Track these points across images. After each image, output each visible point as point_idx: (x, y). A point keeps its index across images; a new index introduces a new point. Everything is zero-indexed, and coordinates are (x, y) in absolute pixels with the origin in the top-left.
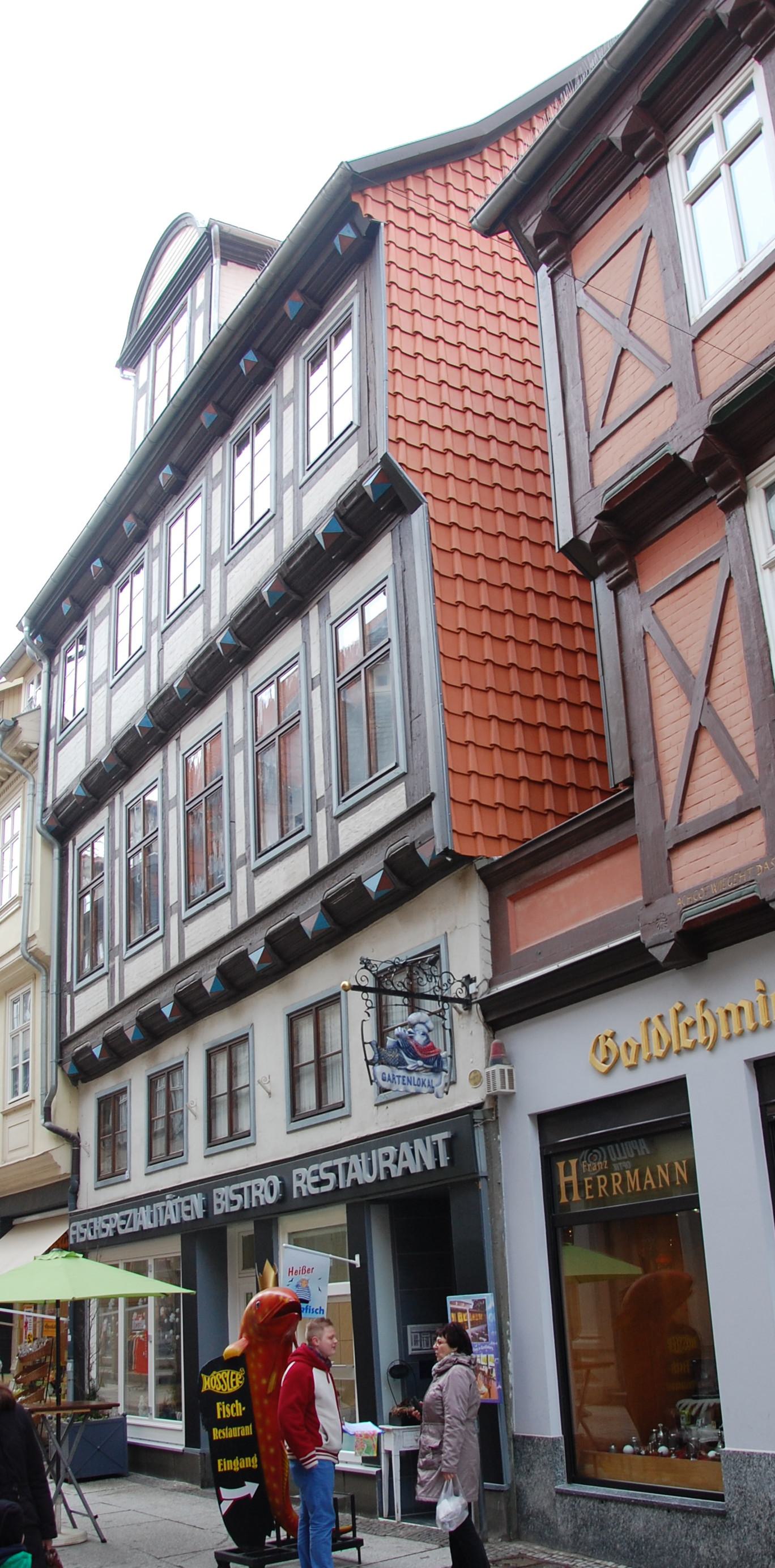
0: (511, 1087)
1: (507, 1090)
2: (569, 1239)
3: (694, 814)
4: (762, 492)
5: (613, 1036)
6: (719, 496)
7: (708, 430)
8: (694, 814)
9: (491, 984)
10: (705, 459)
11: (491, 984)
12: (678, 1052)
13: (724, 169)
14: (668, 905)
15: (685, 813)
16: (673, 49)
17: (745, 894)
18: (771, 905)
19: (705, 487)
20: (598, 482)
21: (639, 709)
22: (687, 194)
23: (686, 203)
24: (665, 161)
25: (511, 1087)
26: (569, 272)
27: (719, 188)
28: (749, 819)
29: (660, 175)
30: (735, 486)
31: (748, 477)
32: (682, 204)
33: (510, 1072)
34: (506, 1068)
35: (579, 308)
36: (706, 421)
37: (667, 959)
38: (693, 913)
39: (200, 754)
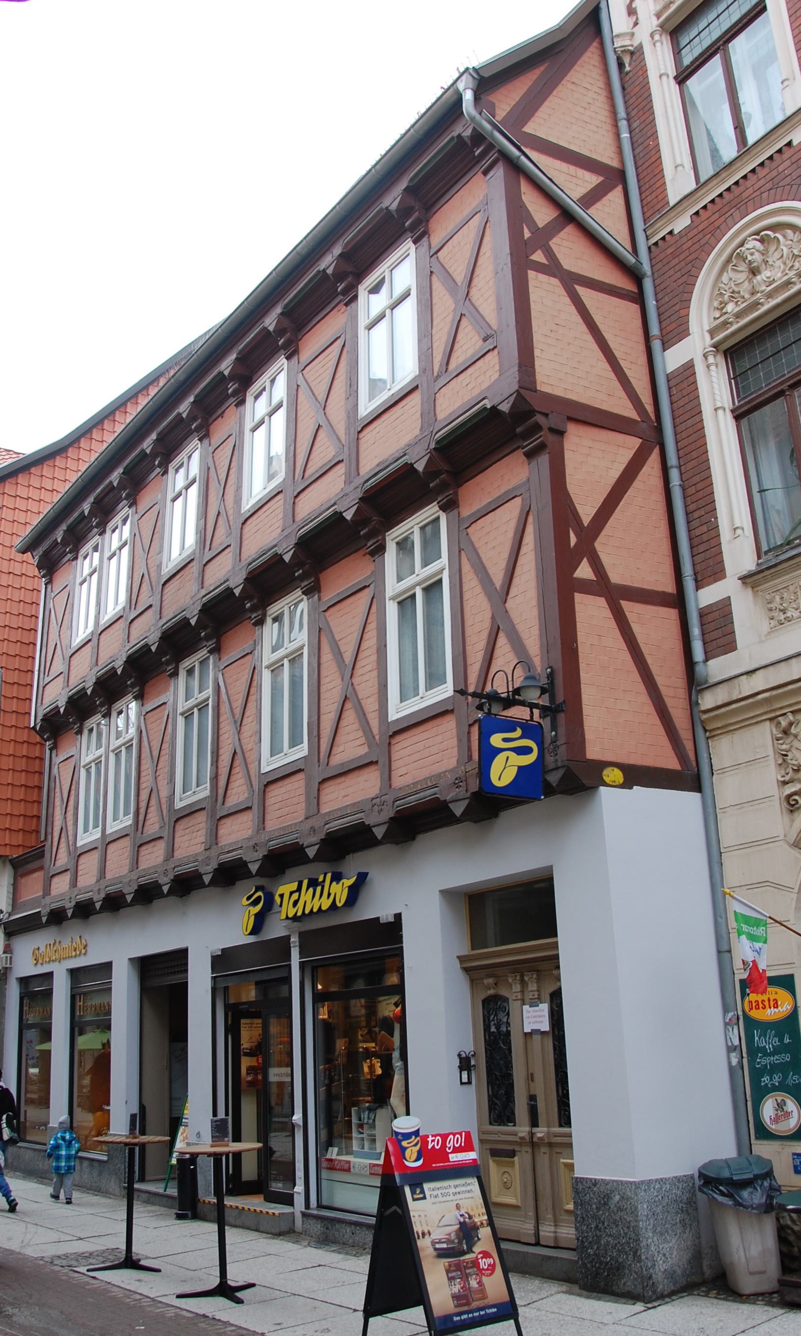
0: (11, 964)
1: (8, 966)
2: (81, 1033)
3: (336, 760)
4: (395, 545)
5: (38, 949)
6: (369, 545)
7: (95, 683)
8: (336, 760)
9: (10, 915)
10: (432, 471)
11: (10, 915)
12: (42, 964)
13: (388, 312)
14: (48, 900)
15: (331, 757)
16: (165, 424)
17: (289, 839)
18: (450, 805)
19: (295, 579)
20: (243, 558)
21: (51, 810)
22: (367, 322)
23: (366, 328)
24: (356, 297)
25: (11, 964)
26: (296, 358)
27: (383, 325)
28: (65, 874)
29: (353, 305)
30: (540, 437)
31: (387, 534)
32: (363, 328)
33: (11, 958)
34: (9, 955)
35: (298, 386)
36: (359, 494)
37: (382, 838)
38: (336, 825)
39: (543, 260)
